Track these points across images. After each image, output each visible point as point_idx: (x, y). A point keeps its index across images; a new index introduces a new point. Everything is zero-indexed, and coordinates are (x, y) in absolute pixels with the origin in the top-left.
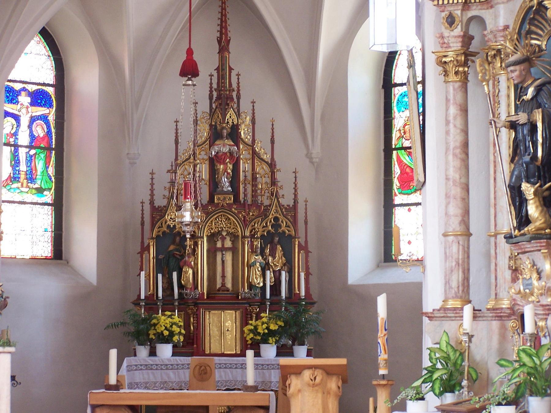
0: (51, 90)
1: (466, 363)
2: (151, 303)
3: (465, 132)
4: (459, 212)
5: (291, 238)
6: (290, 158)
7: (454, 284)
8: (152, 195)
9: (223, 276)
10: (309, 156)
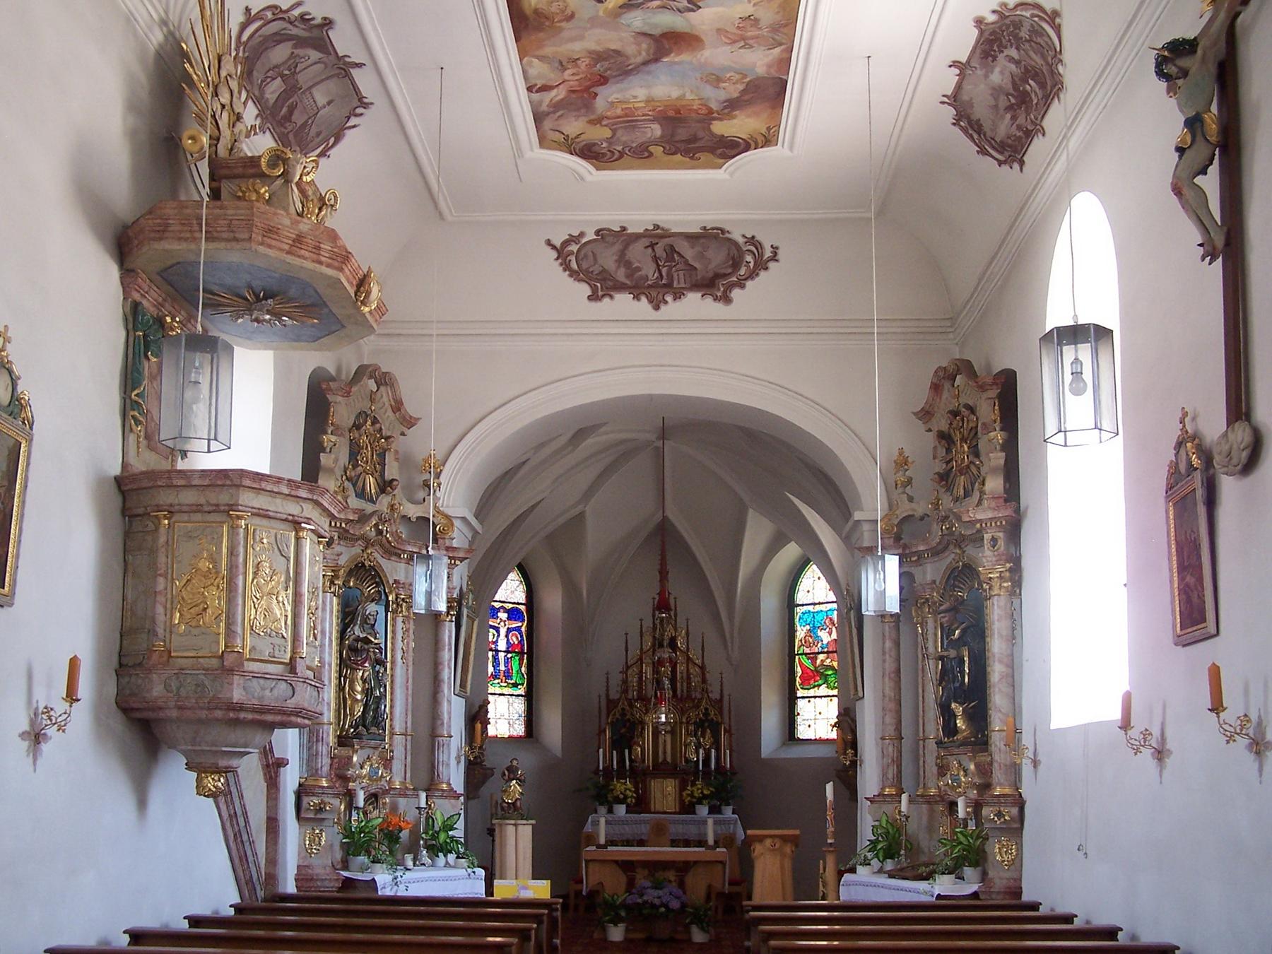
0: (522, 608)
1: (903, 838)
2: (608, 771)
3: (898, 660)
4: (894, 721)
5: (718, 724)
6: (716, 663)
7: (890, 776)
8: (607, 690)
9: (665, 752)
10: (729, 659)
